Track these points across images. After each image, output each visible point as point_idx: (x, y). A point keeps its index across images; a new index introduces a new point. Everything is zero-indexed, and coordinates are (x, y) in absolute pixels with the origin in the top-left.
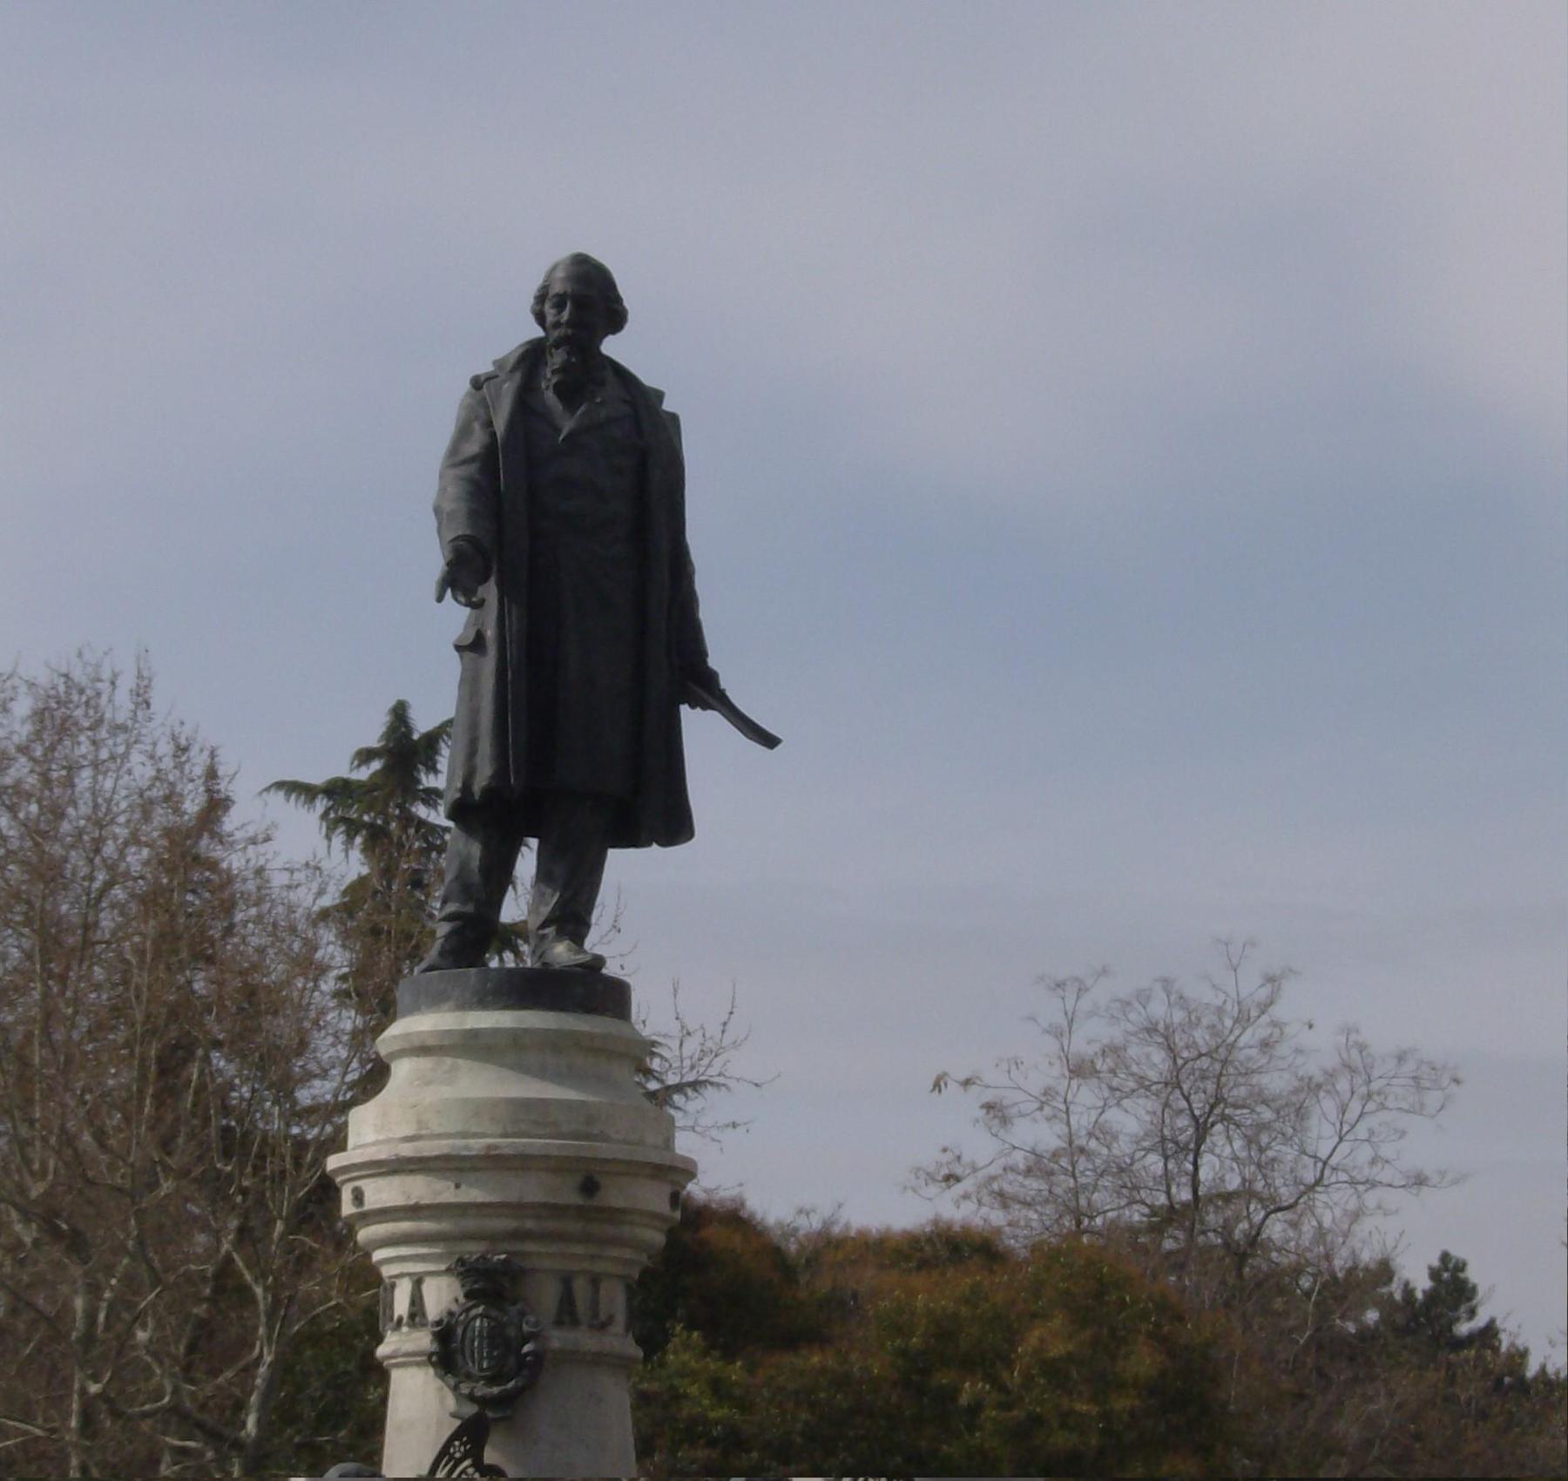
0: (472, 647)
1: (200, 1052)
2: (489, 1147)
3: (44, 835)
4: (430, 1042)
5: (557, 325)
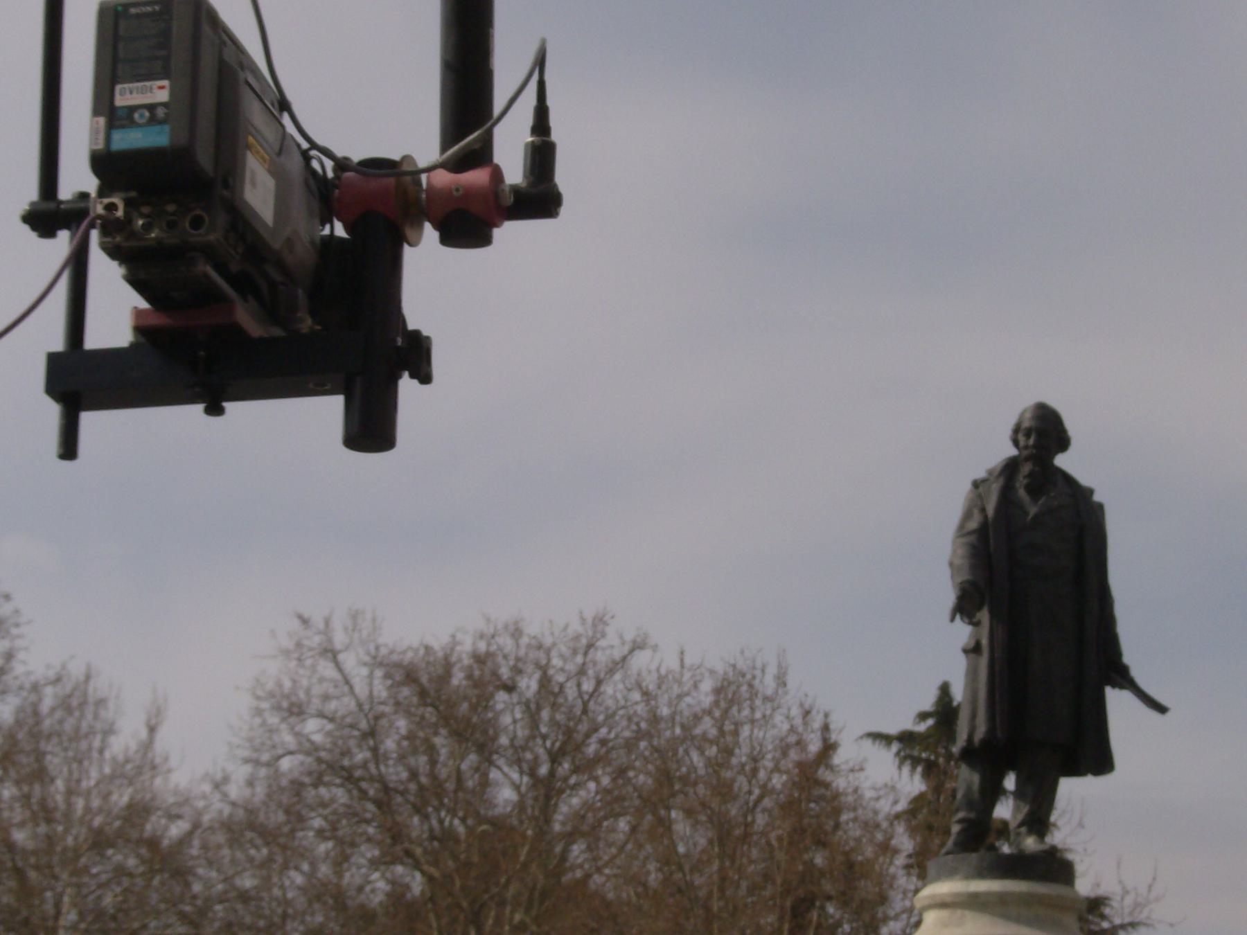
0: (973, 650)
1: (818, 904)
3: (720, 765)
4: (948, 900)
5: (1026, 447)
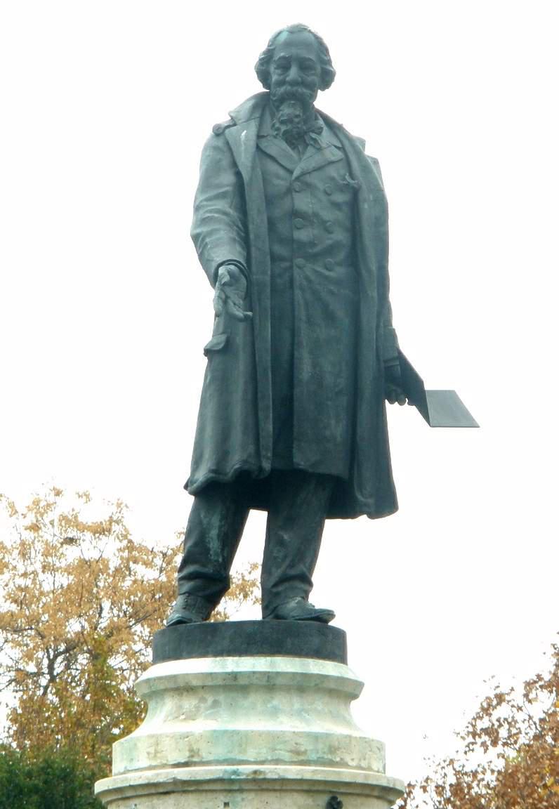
2: (255, 772)
5: (281, 83)
